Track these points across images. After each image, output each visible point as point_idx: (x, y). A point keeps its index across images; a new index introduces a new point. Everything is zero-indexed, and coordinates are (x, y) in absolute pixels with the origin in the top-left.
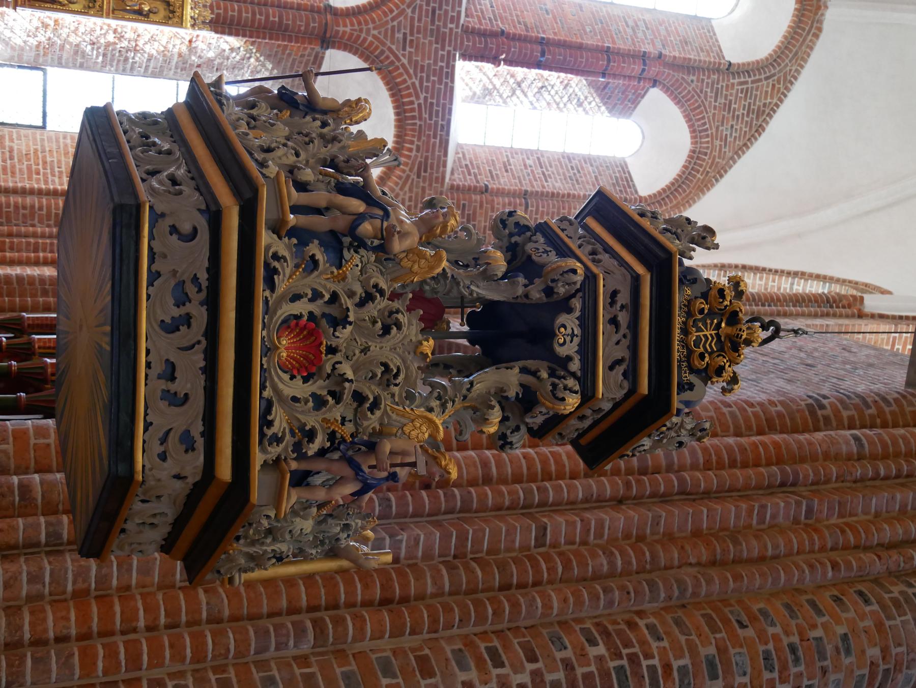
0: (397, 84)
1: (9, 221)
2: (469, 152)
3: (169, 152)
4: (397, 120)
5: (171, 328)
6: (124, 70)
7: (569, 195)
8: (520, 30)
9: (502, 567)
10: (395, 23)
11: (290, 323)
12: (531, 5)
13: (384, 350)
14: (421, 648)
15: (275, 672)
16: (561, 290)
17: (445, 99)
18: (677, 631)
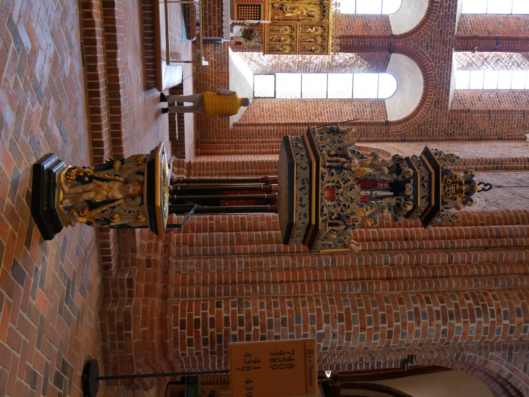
0: (424, 66)
1: (262, 136)
2: (461, 93)
3: (301, 148)
4: (424, 82)
5: (301, 189)
6: (306, 71)
7: (512, 110)
8: (485, 34)
9: (434, 269)
10: (423, 39)
11: (328, 188)
12: (491, 21)
13: (350, 194)
14: (400, 295)
15: (348, 298)
16: (407, 177)
17: (447, 70)
18: (505, 298)
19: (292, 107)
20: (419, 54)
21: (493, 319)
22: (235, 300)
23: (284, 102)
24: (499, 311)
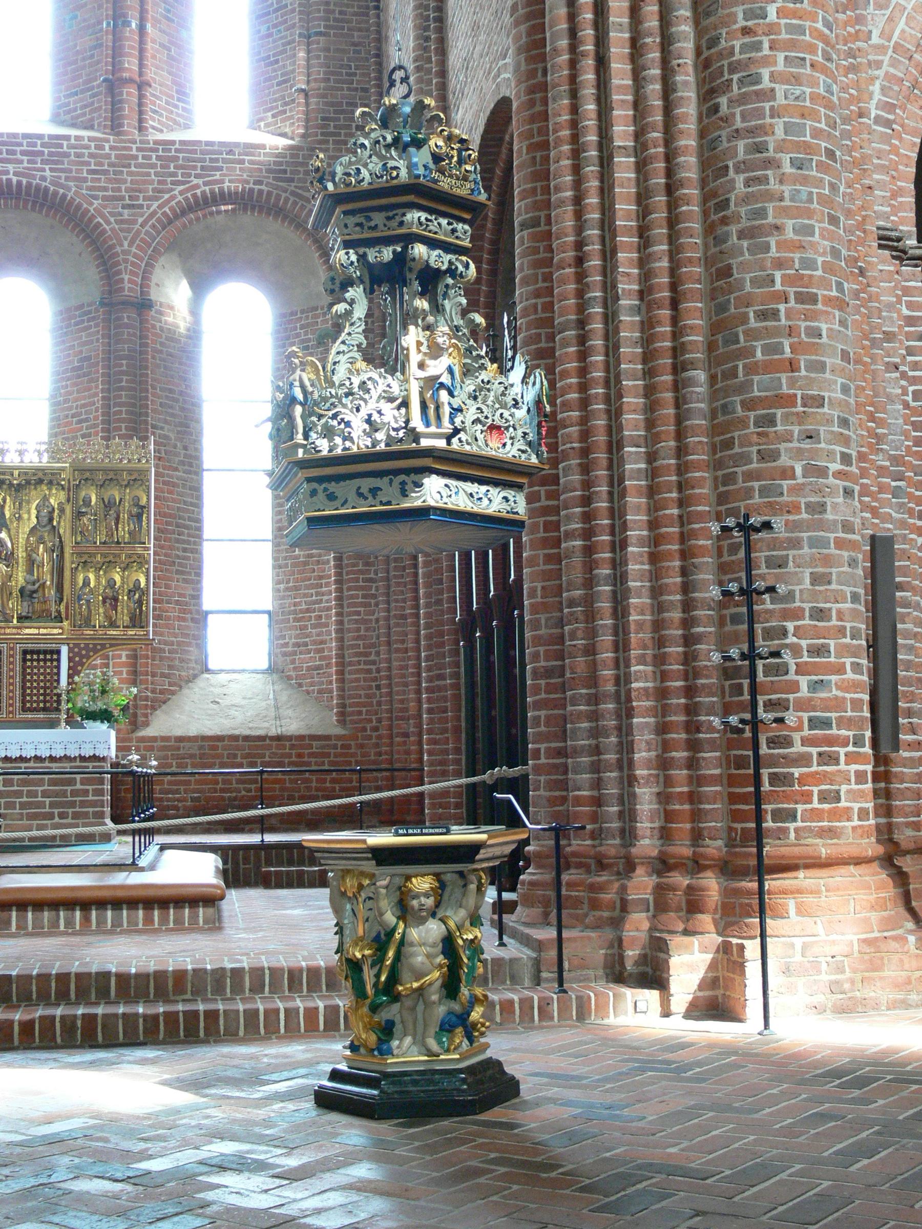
1: (373, 645)
10: (112, 220)
17: (195, 152)
19: (294, 565)
20: (153, 226)
21: (766, 45)
22: (727, 688)
23: (282, 586)
24: (746, 31)
